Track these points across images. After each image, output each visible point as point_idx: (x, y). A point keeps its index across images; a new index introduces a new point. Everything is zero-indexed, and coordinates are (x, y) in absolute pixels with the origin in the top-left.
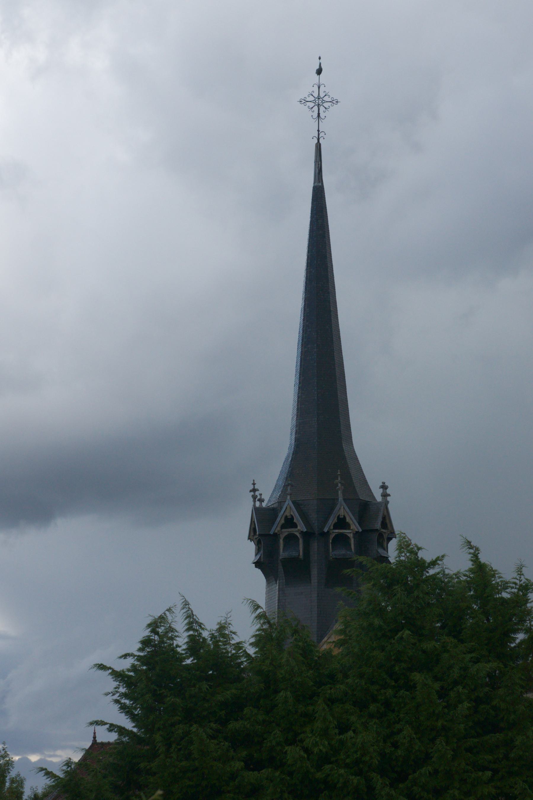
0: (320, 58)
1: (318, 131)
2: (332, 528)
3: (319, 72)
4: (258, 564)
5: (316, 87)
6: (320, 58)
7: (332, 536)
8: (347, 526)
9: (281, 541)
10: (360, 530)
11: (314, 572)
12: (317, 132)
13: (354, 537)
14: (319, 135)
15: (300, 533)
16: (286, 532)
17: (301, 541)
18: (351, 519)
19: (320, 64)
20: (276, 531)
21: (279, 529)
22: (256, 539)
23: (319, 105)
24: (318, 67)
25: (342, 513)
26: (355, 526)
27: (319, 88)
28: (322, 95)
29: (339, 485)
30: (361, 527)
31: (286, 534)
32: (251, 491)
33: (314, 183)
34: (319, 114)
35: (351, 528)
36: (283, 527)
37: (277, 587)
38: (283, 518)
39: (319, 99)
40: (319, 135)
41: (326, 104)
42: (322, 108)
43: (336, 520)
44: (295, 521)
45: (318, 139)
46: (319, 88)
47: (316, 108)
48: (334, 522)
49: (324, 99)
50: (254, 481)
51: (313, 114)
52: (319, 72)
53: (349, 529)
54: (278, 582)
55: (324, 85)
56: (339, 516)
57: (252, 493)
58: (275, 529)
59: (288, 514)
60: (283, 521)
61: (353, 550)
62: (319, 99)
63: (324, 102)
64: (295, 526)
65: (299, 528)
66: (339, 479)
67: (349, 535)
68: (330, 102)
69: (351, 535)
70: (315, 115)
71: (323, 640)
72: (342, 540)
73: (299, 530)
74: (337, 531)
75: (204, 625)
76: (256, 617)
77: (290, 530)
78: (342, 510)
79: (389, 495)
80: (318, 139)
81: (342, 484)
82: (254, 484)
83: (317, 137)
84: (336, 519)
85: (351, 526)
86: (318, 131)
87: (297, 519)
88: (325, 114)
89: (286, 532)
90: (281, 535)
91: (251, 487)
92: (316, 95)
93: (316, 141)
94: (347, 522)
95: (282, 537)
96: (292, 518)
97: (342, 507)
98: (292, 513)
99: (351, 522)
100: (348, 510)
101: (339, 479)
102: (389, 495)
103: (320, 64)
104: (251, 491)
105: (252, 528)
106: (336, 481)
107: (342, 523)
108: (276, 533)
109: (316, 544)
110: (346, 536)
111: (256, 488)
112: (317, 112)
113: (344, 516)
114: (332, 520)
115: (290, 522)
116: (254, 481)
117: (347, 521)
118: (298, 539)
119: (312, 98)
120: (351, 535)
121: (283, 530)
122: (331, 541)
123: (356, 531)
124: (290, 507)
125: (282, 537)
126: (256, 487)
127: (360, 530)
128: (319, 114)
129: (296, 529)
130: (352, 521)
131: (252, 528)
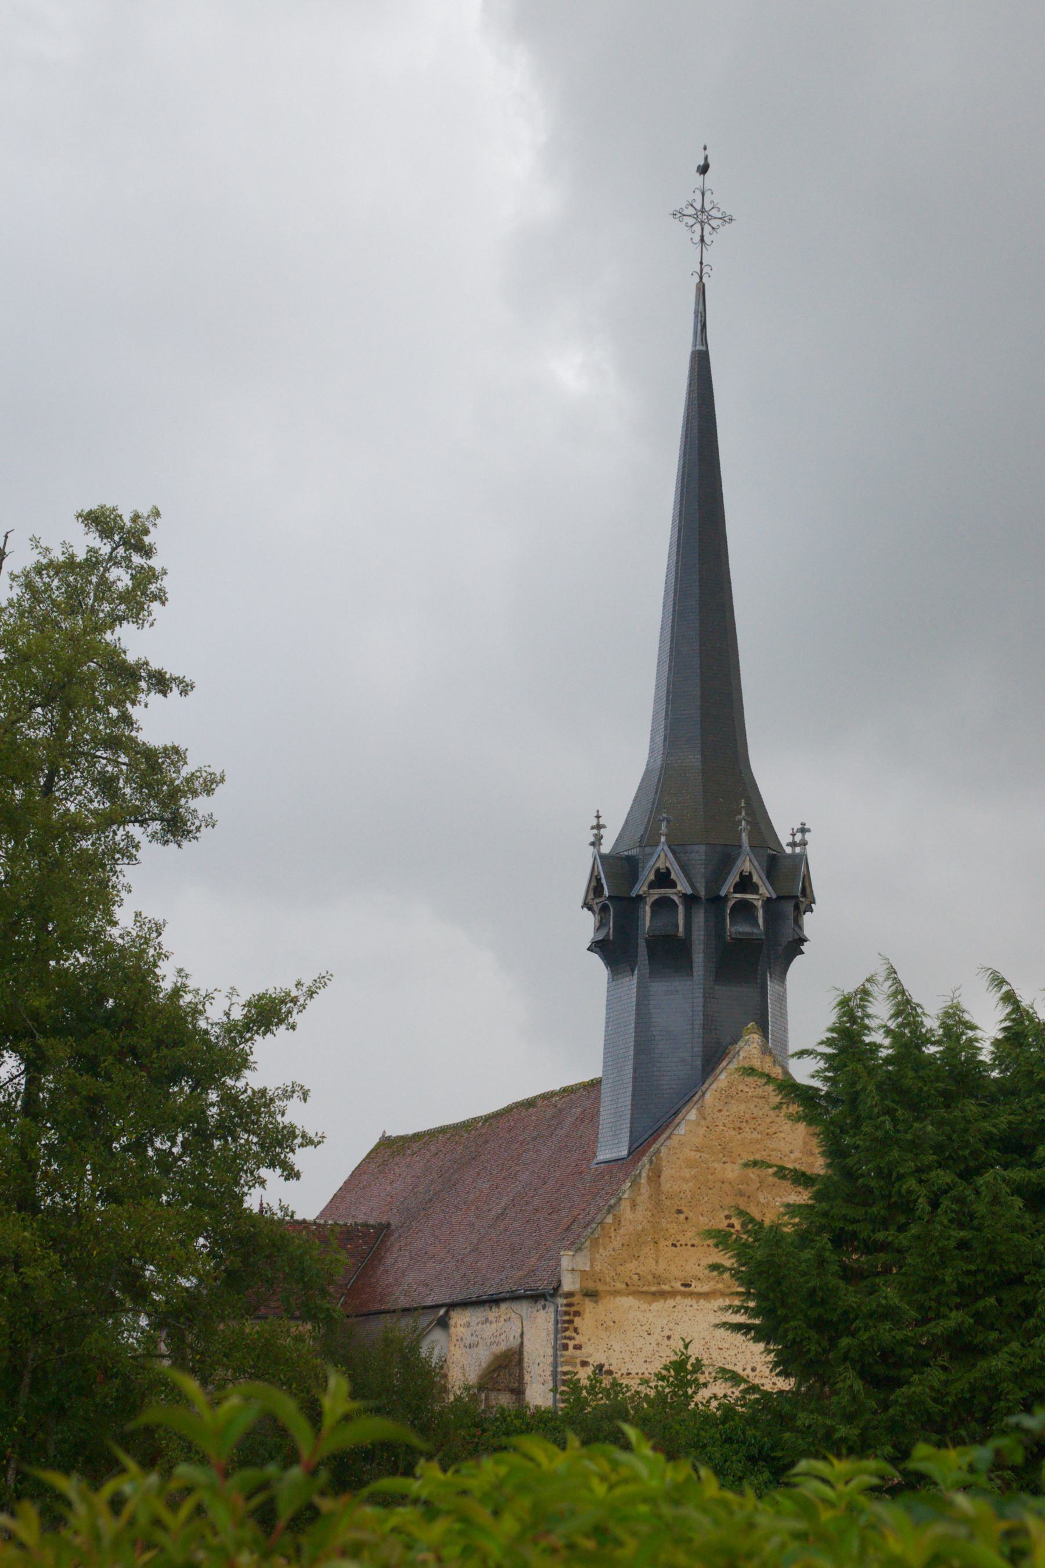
0: (705, 148)
1: (701, 263)
2: (732, 891)
3: (704, 169)
4: (599, 946)
5: (699, 194)
6: (705, 148)
7: (731, 903)
8: (754, 889)
9: (648, 909)
10: (774, 896)
11: (699, 957)
12: (699, 265)
13: (763, 906)
14: (702, 271)
15: (680, 897)
16: (656, 893)
17: (681, 909)
18: (760, 878)
19: (706, 158)
20: (641, 893)
21: (645, 888)
22: (597, 904)
23: (702, 223)
24: (702, 163)
25: (747, 867)
26: (766, 890)
27: (703, 194)
28: (707, 207)
29: (743, 823)
30: (775, 892)
31: (656, 897)
32: (593, 828)
33: (695, 345)
34: (702, 237)
35: (760, 892)
36: (652, 885)
37: (635, 981)
38: (653, 872)
39: (702, 212)
40: (702, 271)
41: (691, 211)
42: (707, 228)
43: (737, 879)
44: (673, 876)
45: (701, 278)
46: (703, 194)
47: (698, 227)
48: (734, 882)
49: (711, 213)
50: (598, 811)
51: (692, 236)
52: (704, 169)
53: (757, 893)
54: (636, 972)
55: (710, 192)
56: (741, 873)
57: (595, 831)
58: (641, 888)
59: (660, 864)
60: (652, 877)
61: (762, 927)
62: (702, 212)
63: (710, 217)
64: (673, 885)
65: (679, 888)
66: (743, 814)
67: (755, 903)
68: (721, 218)
69: (759, 904)
70: (697, 238)
71: (721, 1066)
72: (744, 909)
73: (679, 892)
74: (738, 896)
75: (922, 1008)
76: (1002, 999)
77: (663, 891)
78: (747, 863)
79: (604, 827)
80: (701, 278)
81: (748, 823)
82: (598, 817)
83: (699, 272)
84: (738, 877)
85: (760, 889)
86: (701, 263)
87: (676, 874)
88: (712, 238)
89: (656, 893)
90: (648, 899)
91: (594, 822)
92: (699, 207)
93: (698, 280)
94: (755, 883)
95: (650, 901)
96: (668, 872)
97: (748, 858)
98: (668, 865)
99: (760, 883)
100: (756, 863)
101: (743, 814)
102: (604, 827)
103: (706, 158)
104: (593, 828)
105: (591, 886)
106: (738, 817)
107: (745, 884)
108: (641, 895)
109: (702, 915)
110: (752, 904)
111: (601, 823)
112: (700, 234)
113: (750, 873)
114: (733, 878)
115: (663, 879)
116: (598, 811)
117: (754, 880)
118: (677, 906)
119: (691, 211)
120: (759, 904)
121: (652, 891)
122: (728, 912)
123: (768, 898)
124: (666, 855)
125: (650, 901)
126: (602, 822)
127: (774, 896)
128: (702, 237)
129: (674, 890)
130: (763, 881)
131: (591, 886)
